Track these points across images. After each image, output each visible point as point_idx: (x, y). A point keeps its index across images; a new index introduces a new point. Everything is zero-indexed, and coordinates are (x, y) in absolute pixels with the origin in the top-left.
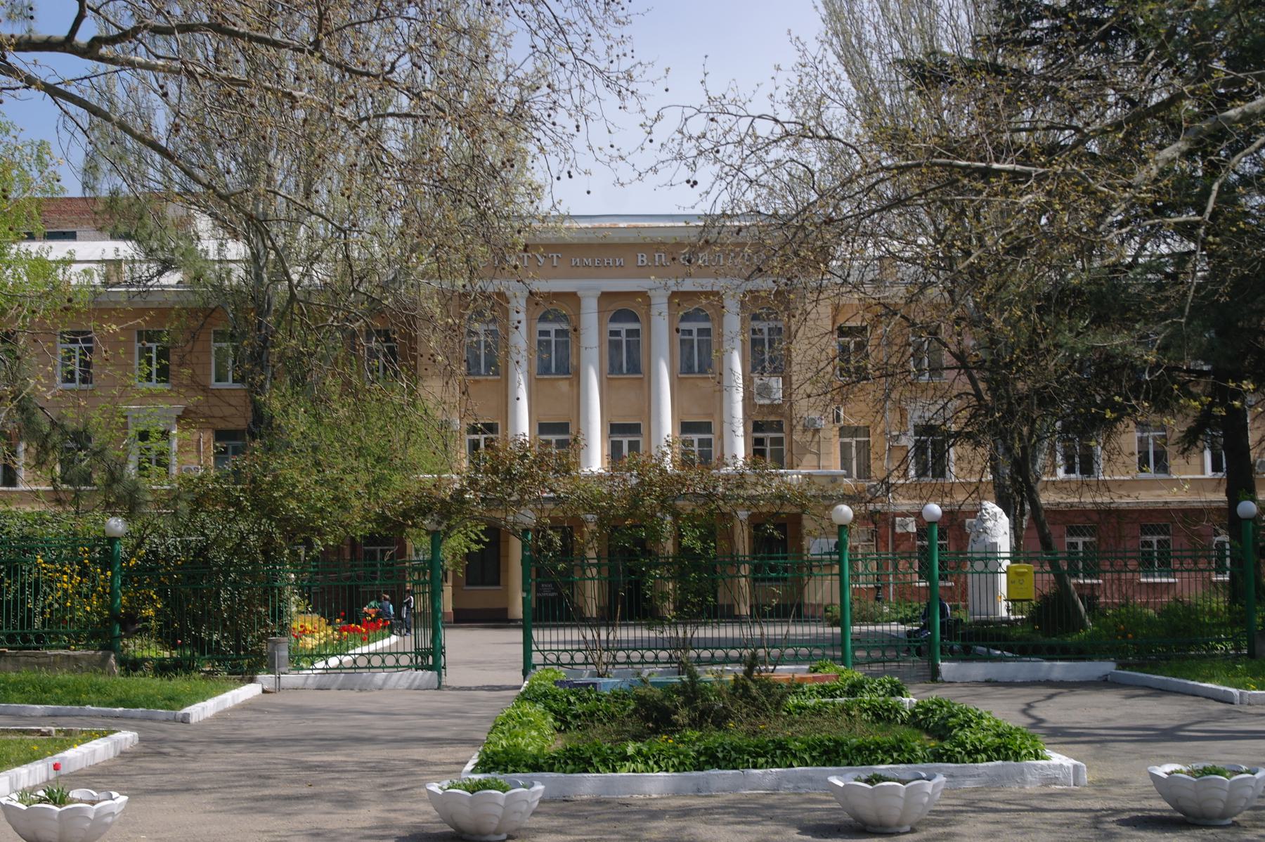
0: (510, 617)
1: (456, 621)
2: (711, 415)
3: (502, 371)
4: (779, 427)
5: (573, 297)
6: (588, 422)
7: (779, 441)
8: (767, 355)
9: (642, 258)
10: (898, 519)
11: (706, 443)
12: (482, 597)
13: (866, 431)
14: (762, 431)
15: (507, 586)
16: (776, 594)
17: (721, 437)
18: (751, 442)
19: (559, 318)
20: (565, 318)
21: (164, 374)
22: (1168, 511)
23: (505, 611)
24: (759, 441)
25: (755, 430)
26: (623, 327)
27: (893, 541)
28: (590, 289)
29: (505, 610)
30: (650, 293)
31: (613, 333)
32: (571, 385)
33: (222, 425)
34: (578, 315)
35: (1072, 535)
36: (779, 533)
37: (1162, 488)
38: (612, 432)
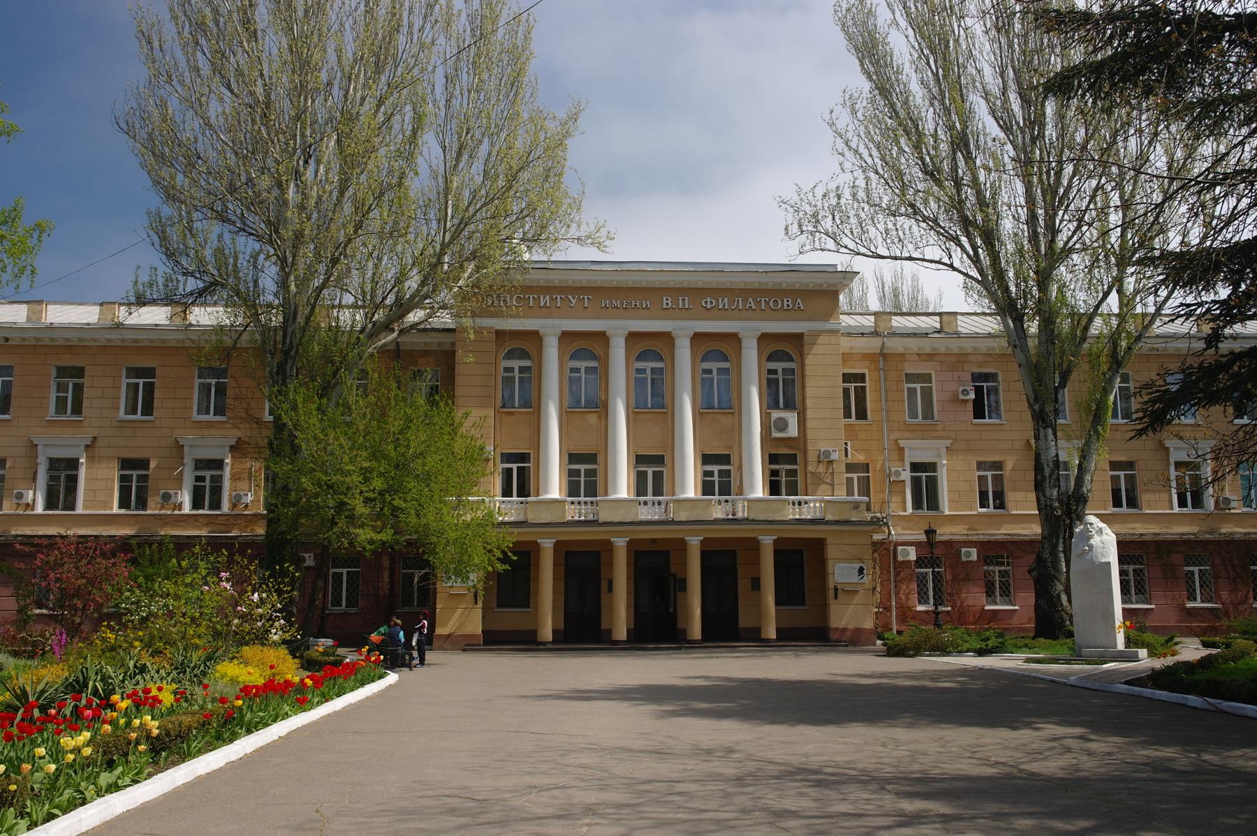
0: (539, 640)
1: (485, 643)
2: (731, 447)
3: (534, 404)
4: (792, 459)
5: (602, 337)
6: (615, 452)
7: (793, 473)
8: (784, 392)
9: (667, 301)
10: (900, 548)
11: (591, 473)
12: (511, 619)
13: (866, 467)
14: (777, 463)
15: (536, 608)
16: (800, 616)
17: (740, 468)
18: (768, 473)
19: (524, 355)
20: (594, 357)
21: (220, 411)
22: (1144, 542)
23: (534, 633)
24: (774, 473)
25: (771, 463)
26: (779, 366)
27: (895, 569)
28: (618, 328)
29: (758, 630)
30: (674, 334)
31: (639, 371)
32: (599, 418)
33: (129, 454)
34: (802, 356)
35: (337, 567)
36: (801, 561)
37: (1135, 522)
38: (637, 462)
